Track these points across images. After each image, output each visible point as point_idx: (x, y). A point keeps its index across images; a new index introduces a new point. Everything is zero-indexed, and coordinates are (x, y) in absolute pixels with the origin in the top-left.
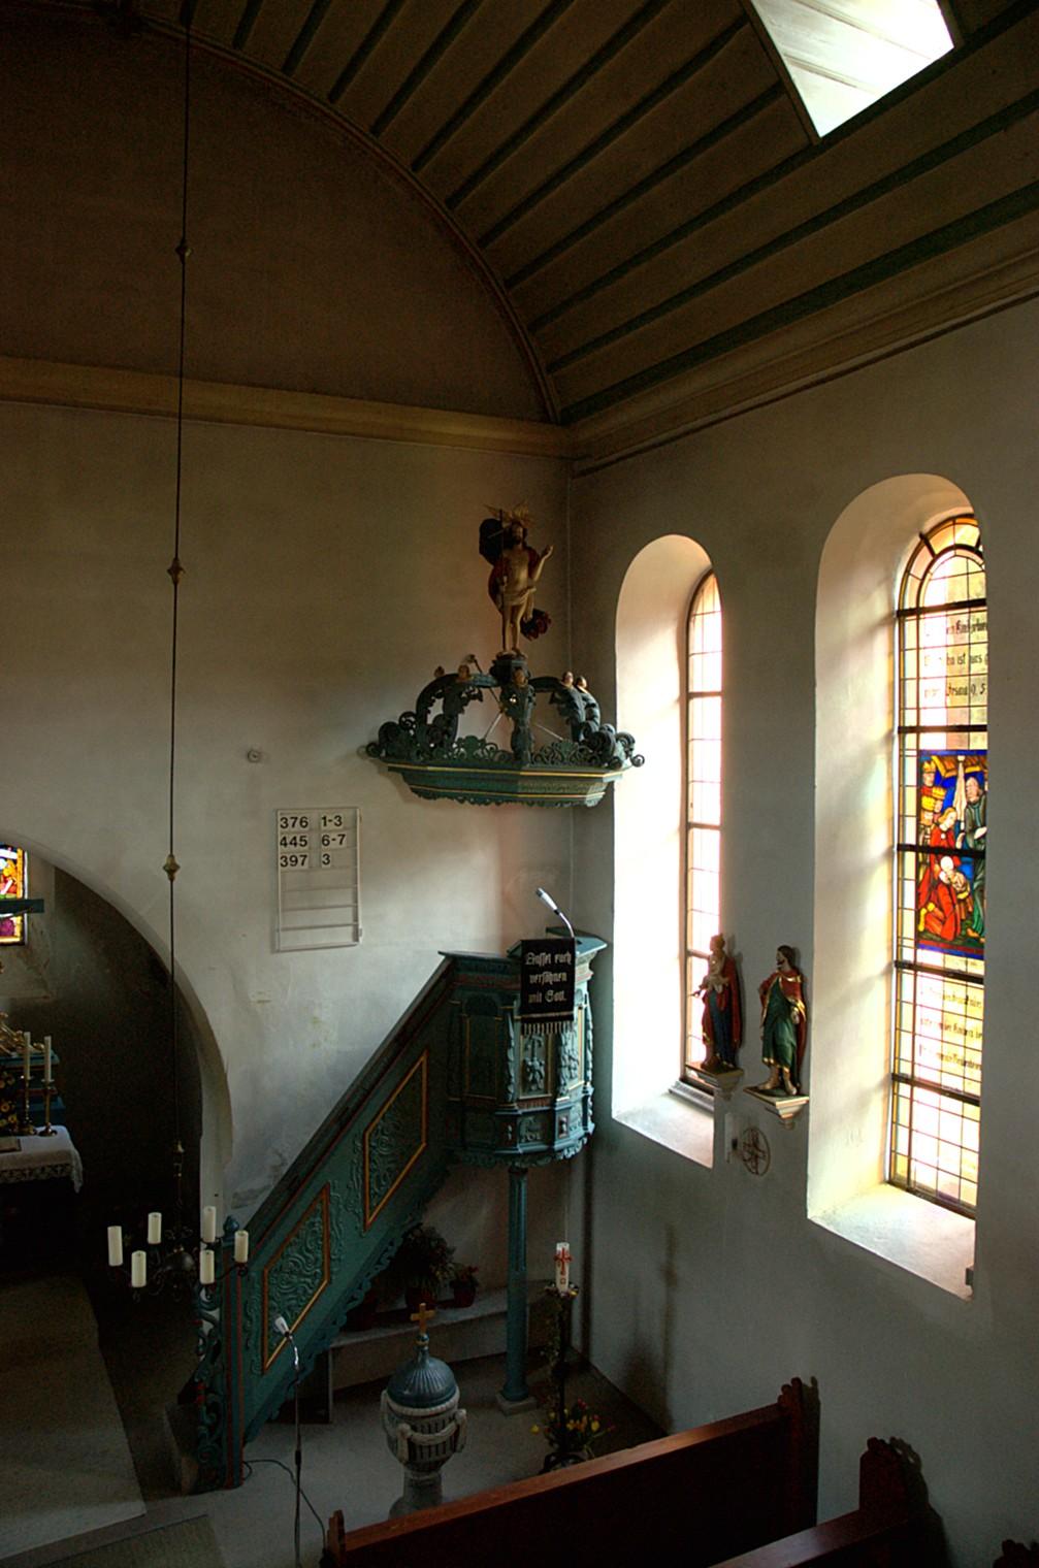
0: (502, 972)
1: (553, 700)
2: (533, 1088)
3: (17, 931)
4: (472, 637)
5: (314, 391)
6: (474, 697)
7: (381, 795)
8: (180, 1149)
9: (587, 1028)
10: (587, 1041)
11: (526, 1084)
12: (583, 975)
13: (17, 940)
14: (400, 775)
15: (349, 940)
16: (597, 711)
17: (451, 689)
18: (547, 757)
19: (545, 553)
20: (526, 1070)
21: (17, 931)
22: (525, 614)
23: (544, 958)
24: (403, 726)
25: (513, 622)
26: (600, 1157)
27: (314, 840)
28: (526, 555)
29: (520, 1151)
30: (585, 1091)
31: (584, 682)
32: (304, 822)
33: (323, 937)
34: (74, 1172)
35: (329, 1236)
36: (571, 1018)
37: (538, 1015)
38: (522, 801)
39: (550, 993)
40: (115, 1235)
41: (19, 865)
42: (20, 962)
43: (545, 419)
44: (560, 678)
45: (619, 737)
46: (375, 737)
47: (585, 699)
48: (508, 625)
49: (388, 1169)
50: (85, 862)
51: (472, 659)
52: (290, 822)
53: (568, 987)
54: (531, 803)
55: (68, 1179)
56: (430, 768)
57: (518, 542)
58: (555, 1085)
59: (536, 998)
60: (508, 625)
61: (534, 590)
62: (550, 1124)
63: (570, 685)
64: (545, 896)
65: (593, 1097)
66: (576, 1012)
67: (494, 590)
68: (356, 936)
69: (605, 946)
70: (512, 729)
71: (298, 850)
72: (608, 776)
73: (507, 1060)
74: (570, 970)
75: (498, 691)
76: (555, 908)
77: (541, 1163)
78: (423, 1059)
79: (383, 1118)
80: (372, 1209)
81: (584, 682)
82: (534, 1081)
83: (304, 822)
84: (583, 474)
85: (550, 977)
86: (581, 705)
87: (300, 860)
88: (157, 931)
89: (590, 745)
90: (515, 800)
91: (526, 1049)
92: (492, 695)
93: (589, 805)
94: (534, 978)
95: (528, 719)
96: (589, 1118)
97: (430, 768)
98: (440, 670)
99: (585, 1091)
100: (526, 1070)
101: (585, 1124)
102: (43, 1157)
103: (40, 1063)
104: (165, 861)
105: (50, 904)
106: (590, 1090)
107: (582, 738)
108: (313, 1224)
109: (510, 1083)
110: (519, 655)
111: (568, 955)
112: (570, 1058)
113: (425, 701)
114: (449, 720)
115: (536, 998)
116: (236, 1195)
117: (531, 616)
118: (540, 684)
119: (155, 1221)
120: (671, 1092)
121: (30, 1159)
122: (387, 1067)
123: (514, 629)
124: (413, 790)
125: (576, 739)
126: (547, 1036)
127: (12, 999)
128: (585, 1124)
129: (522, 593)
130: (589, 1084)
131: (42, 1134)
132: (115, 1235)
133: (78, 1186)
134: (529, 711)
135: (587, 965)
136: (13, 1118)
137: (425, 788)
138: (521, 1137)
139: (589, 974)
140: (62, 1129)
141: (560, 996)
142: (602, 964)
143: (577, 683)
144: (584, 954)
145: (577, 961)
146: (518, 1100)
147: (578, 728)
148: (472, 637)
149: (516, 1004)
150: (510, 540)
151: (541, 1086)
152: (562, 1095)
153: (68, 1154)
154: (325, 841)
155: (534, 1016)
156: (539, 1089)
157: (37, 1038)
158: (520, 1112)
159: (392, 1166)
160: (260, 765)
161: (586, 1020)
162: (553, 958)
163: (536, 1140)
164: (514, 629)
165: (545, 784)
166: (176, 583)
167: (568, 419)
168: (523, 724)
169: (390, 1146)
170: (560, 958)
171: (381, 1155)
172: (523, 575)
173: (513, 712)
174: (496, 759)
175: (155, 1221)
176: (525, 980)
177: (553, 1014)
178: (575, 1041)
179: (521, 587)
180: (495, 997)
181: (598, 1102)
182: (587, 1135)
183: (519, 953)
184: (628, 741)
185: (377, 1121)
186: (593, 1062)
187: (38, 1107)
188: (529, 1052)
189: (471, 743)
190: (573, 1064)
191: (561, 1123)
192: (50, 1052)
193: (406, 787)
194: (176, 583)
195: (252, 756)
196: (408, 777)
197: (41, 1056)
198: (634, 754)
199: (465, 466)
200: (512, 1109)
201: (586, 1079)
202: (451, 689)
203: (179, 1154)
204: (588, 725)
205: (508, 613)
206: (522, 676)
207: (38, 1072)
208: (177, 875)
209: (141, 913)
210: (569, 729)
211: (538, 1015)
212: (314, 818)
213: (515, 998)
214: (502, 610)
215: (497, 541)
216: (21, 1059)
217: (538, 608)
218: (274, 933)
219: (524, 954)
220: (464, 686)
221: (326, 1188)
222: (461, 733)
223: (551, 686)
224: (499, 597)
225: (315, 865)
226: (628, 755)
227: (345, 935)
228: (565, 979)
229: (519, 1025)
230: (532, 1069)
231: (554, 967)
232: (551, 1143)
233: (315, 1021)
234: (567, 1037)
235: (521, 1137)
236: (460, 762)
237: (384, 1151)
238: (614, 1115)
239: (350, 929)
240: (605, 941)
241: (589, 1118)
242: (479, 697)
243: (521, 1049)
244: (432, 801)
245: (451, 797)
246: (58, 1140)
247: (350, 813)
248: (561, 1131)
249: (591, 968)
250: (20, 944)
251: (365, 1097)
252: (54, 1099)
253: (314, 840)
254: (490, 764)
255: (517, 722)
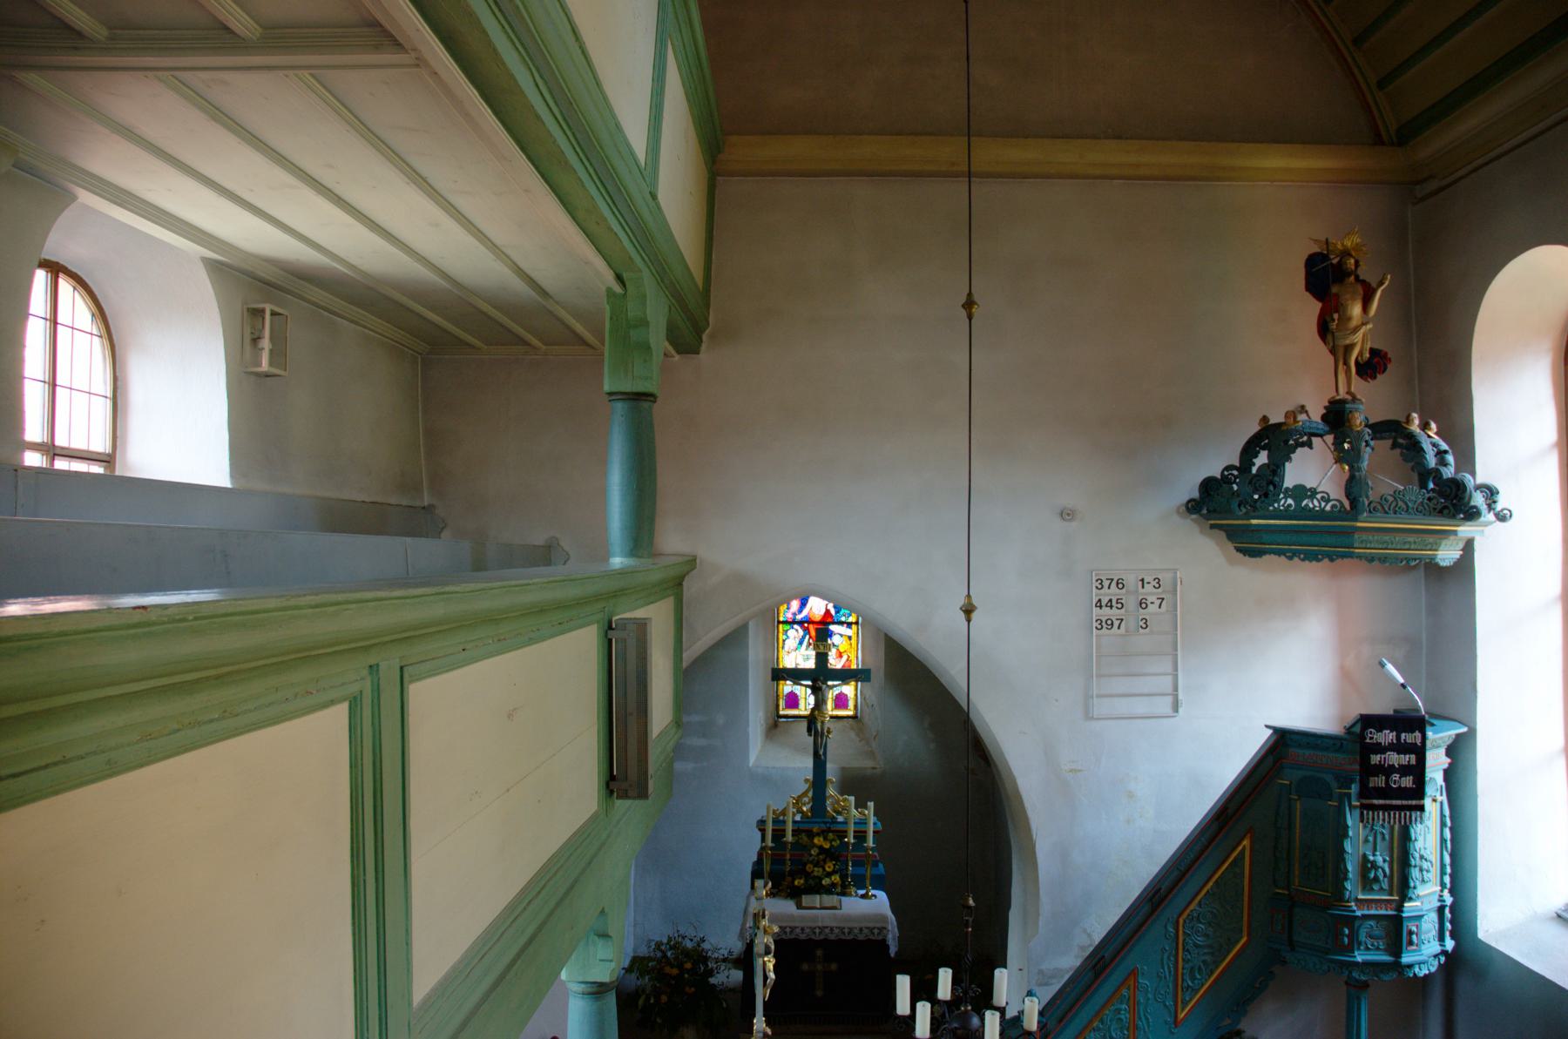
0: (1336, 751)
1: (1394, 446)
2: (1376, 887)
3: (851, 704)
4: (1305, 388)
5: (1119, 137)
6: (1303, 445)
7: (1203, 556)
8: (971, 902)
9: (1443, 824)
10: (1443, 840)
11: (1367, 882)
12: (1436, 762)
13: (851, 713)
14: (1223, 534)
15: (1168, 710)
16: (1450, 458)
17: (1277, 439)
18: (1384, 507)
19: (1381, 283)
20: (1366, 866)
21: (851, 704)
22: (1361, 353)
23: (1387, 737)
24: (1225, 480)
25: (1346, 363)
26: (1464, 984)
27: (1131, 603)
28: (1360, 290)
29: (1359, 959)
30: (1441, 900)
31: (1433, 426)
32: (1120, 584)
33: (1140, 706)
34: (890, 936)
35: (1135, 1027)
36: (1421, 808)
37: (1381, 802)
38: (1360, 557)
39: (1396, 777)
40: (903, 983)
41: (854, 641)
42: (853, 735)
43: (1378, 141)
44: (1403, 419)
45: (1478, 487)
46: (1196, 494)
47: (1434, 445)
48: (1341, 366)
49: (1204, 962)
50: (904, 623)
51: (1303, 409)
52: (1106, 583)
53: (1418, 771)
54: (1371, 559)
55: (883, 944)
56: (1254, 522)
57: (1349, 275)
58: (1403, 888)
59: (1378, 781)
60: (1341, 366)
61: (1369, 326)
62: (1396, 932)
63: (1415, 427)
64: (1390, 667)
65: (1453, 908)
66: (1427, 802)
67: (1324, 330)
68: (1176, 707)
69: (1465, 729)
70: (1347, 475)
71: (1114, 613)
72: (1465, 530)
73: (1343, 851)
74: (1420, 752)
75: (1330, 439)
76: (1401, 680)
77: (1386, 978)
78: (1246, 842)
79: (1200, 904)
80: (1185, 1004)
81: (1433, 426)
82: (1376, 879)
83: (1120, 584)
84: (1423, 199)
85: (1394, 759)
86: (1426, 446)
87: (1116, 623)
88: (951, 670)
89: (1441, 494)
90: (1350, 556)
91: (1366, 841)
92: (1322, 447)
93: (1442, 564)
94: (1375, 759)
95: (1365, 464)
96: (1447, 934)
97: (1254, 522)
98: (1265, 419)
99: (1441, 900)
100: (1366, 866)
101: (1441, 938)
102: (865, 917)
103: (862, 828)
104: (961, 601)
105: (878, 676)
106: (1449, 900)
107: (1431, 486)
108: (1118, 1011)
109: (1346, 878)
110: (1354, 399)
111: (1418, 734)
112: (1422, 857)
113: (1249, 450)
114: (1275, 470)
115: (1378, 781)
116: (1041, 972)
117: (1367, 355)
118: (1382, 429)
119: (945, 977)
120: (1559, 916)
121: (848, 918)
122: (1207, 847)
123: (1348, 371)
124: (1238, 550)
125: (1423, 485)
126: (1392, 828)
127: (843, 769)
128: (1441, 938)
129: (1356, 330)
130: (1446, 892)
131: (863, 896)
132: (903, 983)
133: (893, 951)
134: (1366, 456)
135: (1443, 751)
136: (836, 878)
137: (1249, 545)
138: (1360, 944)
139: (1445, 761)
140: (882, 896)
141: (1407, 782)
142: (1460, 750)
143: (1425, 426)
144: (1438, 737)
145: (1428, 743)
146: (1357, 900)
147: (1424, 475)
148: (1305, 388)
149: (1354, 789)
150: (1340, 273)
151: (1385, 886)
152: (1411, 899)
153: (884, 918)
154: (1142, 604)
155: (1376, 802)
156: (1381, 889)
157: (860, 804)
158: (1359, 913)
159: (1208, 958)
160: (1074, 524)
161: (1442, 816)
162: (1398, 738)
163: (1378, 949)
164: (1348, 371)
165: (1387, 538)
166: (970, 317)
167: (1405, 135)
168: (1359, 469)
169: (1207, 936)
170: (1407, 737)
171: (1196, 946)
172: (1356, 310)
173: (1346, 457)
174: (1328, 508)
175: (945, 977)
176: (1365, 760)
177: (1398, 802)
178: (1427, 836)
179: (1354, 323)
180: (1329, 778)
181: (1458, 915)
182: (1444, 952)
183: (1357, 729)
184: (1491, 493)
185: (1192, 907)
186: (1452, 865)
187: (860, 871)
188: (1370, 845)
189: (1300, 492)
190: (1425, 865)
191: (1410, 933)
192: (872, 819)
193: (1230, 546)
194: (970, 317)
195: (1066, 514)
196: (1233, 534)
197: (863, 822)
198: (1499, 507)
199: (1286, 200)
200: (1348, 909)
201: (1443, 885)
202: (1277, 439)
203: (969, 907)
204: (1437, 471)
205: (1340, 353)
206: (1358, 420)
207: (861, 836)
208: (974, 616)
209: (953, 673)
210: (1415, 477)
211: (1381, 802)
212: (1131, 580)
213: (1352, 781)
214: (1333, 351)
215: (1326, 277)
216: (845, 823)
217: (1376, 346)
218: (1088, 697)
219: (1364, 729)
220: (1290, 433)
221: (1134, 973)
222: (1289, 482)
223: (1392, 430)
224: (1329, 337)
225: (1125, 617)
226: (1490, 508)
227: (1164, 705)
228: (1413, 762)
229: (1357, 813)
230: (1374, 864)
231: (1401, 748)
232: (1397, 953)
233: (1131, 795)
234: (1417, 830)
235: (1360, 944)
236: (1286, 514)
237: (1200, 940)
238: (1481, 935)
239: (1169, 699)
240: (1464, 725)
241: (1447, 934)
242: (1309, 445)
243: (1360, 840)
244: (1258, 560)
245: (1279, 553)
246: (878, 904)
247: (1169, 575)
248: (1410, 943)
249: (1448, 754)
250: (854, 717)
251: (1183, 875)
252: (876, 865)
253: (1131, 603)
254: (1321, 515)
255: (1352, 468)
